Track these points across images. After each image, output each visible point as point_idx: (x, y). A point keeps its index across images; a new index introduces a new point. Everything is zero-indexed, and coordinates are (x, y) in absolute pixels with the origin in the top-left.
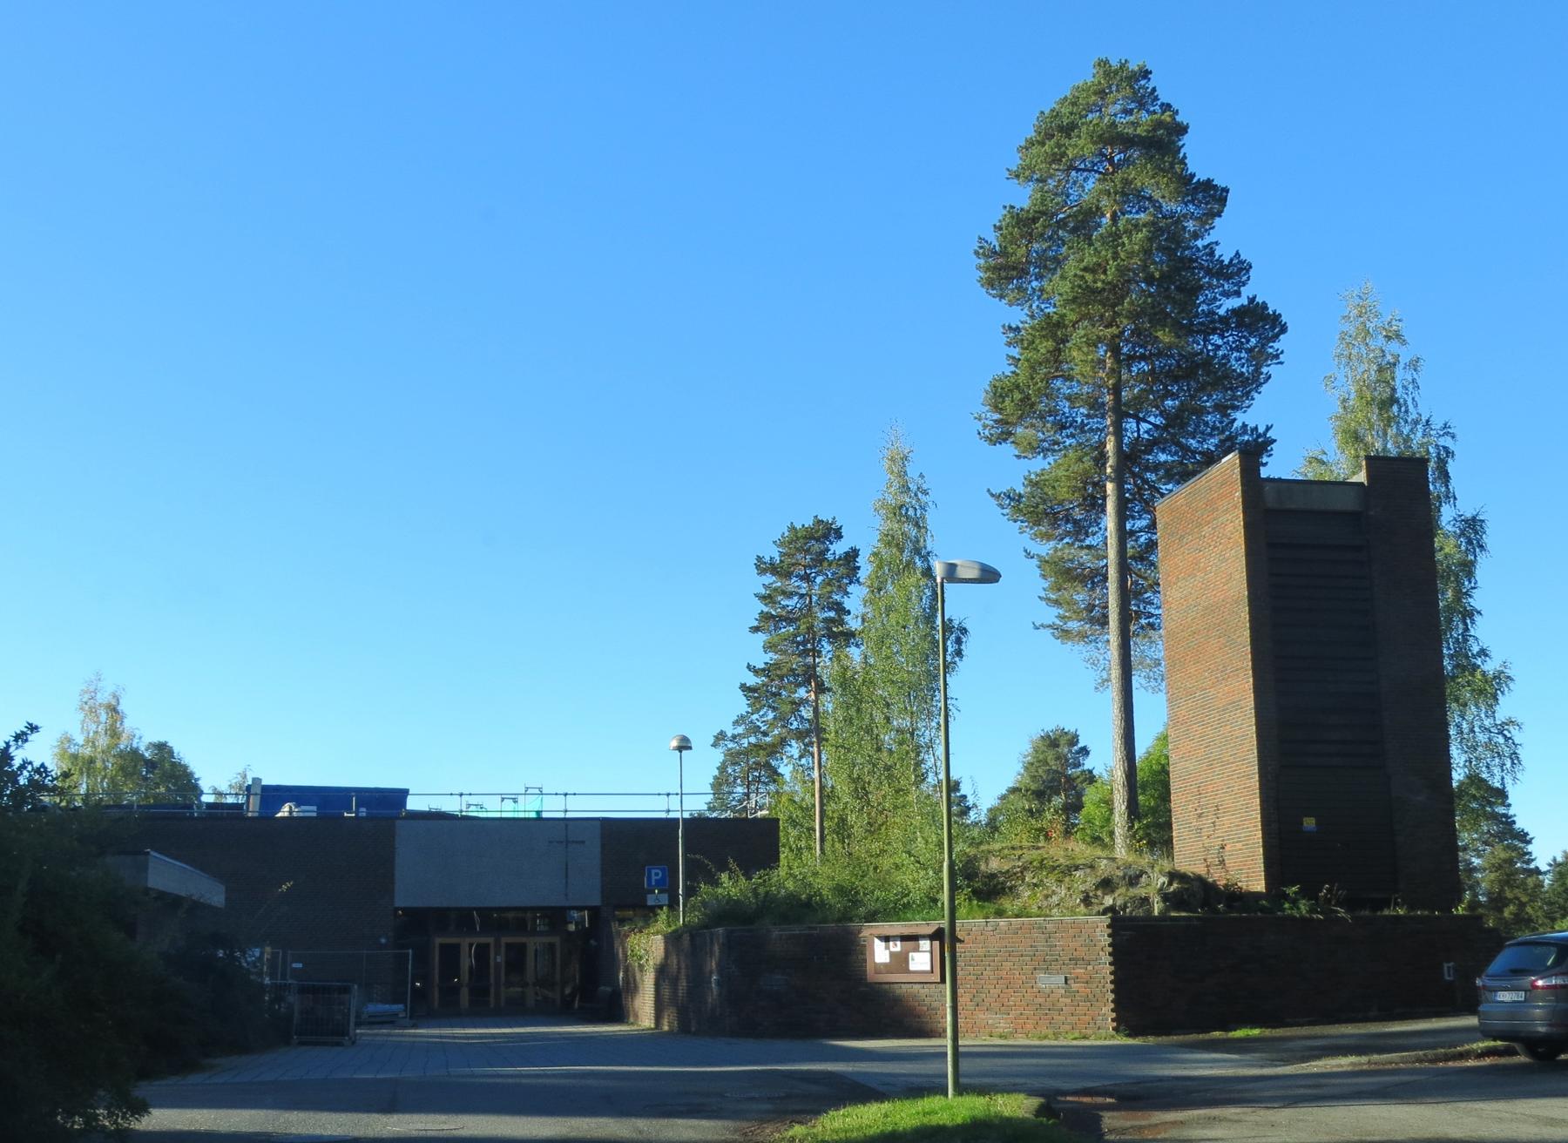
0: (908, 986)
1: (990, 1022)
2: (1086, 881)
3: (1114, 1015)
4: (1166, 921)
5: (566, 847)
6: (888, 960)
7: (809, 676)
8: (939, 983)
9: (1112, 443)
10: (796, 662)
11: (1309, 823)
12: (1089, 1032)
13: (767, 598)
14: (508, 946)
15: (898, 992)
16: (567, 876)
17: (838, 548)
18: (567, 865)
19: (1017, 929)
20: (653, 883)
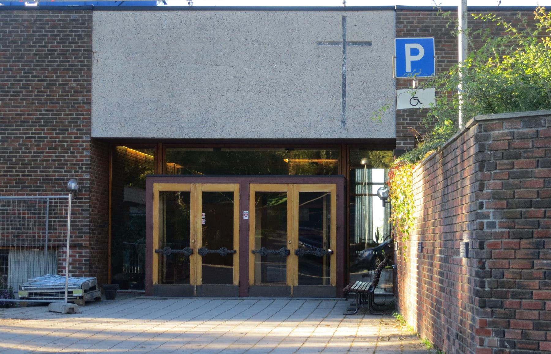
5: (344, 52)
14: (262, 197)
16: (344, 95)
18: (344, 78)
20: (408, 68)
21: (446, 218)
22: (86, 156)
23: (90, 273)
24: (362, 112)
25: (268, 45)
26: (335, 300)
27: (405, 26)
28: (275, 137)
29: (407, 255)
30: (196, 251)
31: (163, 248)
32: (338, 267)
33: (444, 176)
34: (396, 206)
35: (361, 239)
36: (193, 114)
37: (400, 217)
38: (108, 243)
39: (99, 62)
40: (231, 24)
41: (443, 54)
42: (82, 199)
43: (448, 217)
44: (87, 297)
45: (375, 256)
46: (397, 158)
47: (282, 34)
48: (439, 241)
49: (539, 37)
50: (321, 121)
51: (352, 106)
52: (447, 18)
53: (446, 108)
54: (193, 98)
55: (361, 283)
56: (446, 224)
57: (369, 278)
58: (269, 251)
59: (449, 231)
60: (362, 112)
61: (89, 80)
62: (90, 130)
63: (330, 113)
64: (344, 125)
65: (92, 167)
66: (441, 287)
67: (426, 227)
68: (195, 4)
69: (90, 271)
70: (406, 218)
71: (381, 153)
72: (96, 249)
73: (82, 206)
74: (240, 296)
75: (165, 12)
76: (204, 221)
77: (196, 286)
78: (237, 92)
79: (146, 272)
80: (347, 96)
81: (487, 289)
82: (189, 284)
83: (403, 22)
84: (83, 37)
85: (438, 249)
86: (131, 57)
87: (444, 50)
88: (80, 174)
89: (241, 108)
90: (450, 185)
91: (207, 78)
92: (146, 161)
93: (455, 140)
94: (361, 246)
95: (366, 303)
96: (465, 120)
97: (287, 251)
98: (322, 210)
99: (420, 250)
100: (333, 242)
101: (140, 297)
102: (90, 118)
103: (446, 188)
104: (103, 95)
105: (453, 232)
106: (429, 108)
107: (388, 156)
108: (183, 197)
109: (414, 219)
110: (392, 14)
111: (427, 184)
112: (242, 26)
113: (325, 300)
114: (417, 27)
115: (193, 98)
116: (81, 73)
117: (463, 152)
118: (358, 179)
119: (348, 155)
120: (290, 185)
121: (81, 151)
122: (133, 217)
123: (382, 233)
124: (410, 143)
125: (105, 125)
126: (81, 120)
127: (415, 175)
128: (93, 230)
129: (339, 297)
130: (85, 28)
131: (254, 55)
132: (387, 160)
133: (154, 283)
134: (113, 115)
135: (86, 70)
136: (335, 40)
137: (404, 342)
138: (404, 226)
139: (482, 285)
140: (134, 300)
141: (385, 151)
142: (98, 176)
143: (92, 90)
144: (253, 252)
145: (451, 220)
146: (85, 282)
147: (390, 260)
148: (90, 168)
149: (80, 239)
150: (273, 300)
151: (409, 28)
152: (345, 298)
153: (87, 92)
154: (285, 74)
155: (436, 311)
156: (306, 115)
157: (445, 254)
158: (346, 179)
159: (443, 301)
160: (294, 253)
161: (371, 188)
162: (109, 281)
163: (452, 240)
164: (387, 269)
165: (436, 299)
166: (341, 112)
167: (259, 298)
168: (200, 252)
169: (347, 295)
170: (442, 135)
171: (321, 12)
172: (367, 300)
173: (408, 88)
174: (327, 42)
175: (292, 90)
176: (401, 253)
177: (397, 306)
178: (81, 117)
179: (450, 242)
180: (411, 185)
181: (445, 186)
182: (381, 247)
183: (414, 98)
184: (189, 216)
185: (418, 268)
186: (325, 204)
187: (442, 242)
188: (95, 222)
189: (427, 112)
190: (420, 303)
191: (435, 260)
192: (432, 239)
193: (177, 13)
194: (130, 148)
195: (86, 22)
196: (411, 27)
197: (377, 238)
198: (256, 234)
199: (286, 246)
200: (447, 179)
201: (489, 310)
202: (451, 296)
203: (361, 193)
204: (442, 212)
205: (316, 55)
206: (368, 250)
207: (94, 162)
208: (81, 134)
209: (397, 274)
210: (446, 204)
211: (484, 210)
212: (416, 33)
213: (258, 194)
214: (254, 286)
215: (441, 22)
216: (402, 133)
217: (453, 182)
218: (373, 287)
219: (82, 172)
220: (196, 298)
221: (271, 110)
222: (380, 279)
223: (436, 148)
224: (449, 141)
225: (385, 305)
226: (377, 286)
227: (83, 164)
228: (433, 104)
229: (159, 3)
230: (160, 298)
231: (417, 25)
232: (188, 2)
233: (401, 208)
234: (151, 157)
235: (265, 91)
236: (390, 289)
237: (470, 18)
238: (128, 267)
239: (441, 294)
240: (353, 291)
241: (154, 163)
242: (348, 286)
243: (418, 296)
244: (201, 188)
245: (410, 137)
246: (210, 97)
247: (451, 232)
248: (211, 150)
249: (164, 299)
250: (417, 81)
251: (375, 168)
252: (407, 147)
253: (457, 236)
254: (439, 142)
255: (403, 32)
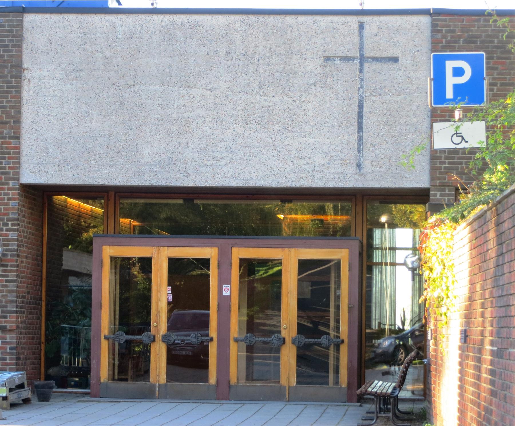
5: (361, 71)
16: (360, 128)
18: (361, 106)
20: (449, 94)
21: (500, 297)
22: (12, 209)
23: (16, 365)
24: (384, 152)
25: (258, 60)
26: (345, 405)
27: (444, 37)
28: (267, 185)
29: (444, 346)
30: (159, 337)
31: (114, 334)
32: (350, 361)
33: (498, 241)
34: (431, 279)
35: (380, 324)
36: (157, 154)
37: (435, 294)
38: (41, 325)
39: (31, 83)
40: (209, 32)
41: (495, 74)
42: (6, 266)
43: (502, 296)
44: (13, 398)
45: (397, 348)
46: (432, 215)
47: (276, 46)
48: (491, 328)
50: (329, 164)
51: (371, 144)
52: (504, 26)
53: (500, 148)
54: (157, 132)
55: (381, 383)
56: (499, 305)
57: (390, 377)
58: (257, 339)
59: (504, 315)
60: (384, 152)
61: (17, 106)
62: (18, 174)
63: (342, 152)
64: (360, 170)
65: (21, 224)
66: (491, 390)
67: (472, 309)
68: (161, 5)
69: (16, 363)
70: (445, 297)
71: (408, 207)
72: (25, 334)
73: (7, 276)
74: (218, 399)
75: (120, 16)
76: (170, 298)
77: (159, 385)
78: (215, 124)
79: (92, 366)
80: (364, 130)
82: (149, 382)
83: (440, 31)
84: (10, 48)
85: (488, 339)
86: (74, 75)
87: (496, 69)
88: (4, 232)
89: (221, 146)
90: (506, 252)
91: (175, 105)
92: (93, 216)
94: (380, 333)
95: (388, 410)
97: (282, 339)
98: (328, 283)
99: (463, 340)
100: (344, 328)
101: (83, 399)
102: (19, 158)
103: (501, 257)
104: (36, 127)
105: (509, 316)
106: (478, 148)
107: (417, 211)
108: (140, 264)
109: (455, 297)
110: (425, 21)
111: (473, 252)
112: (224, 35)
113: (332, 405)
114: (460, 37)
115: (157, 132)
116: (7, 97)
118: (377, 242)
119: (365, 209)
120: (287, 250)
121: (6, 201)
122: (74, 291)
123: (408, 318)
124: (449, 195)
125: (38, 166)
126: (7, 159)
127: (456, 238)
128: (22, 307)
129: (351, 402)
130: (13, 36)
131: (239, 74)
132: (415, 217)
133: (102, 381)
134: (49, 154)
135: (14, 93)
136: (349, 54)
138: (441, 306)
140: (76, 402)
141: (414, 205)
142: (28, 235)
143: (21, 120)
144: (236, 340)
145: (507, 301)
146: (10, 378)
147: (421, 353)
148: (19, 225)
149: (4, 320)
150: (262, 406)
151: (449, 38)
152: (359, 404)
153: (14, 122)
154: (281, 100)
155: (484, 423)
156: (308, 156)
157: (498, 345)
158: (361, 243)
159: (495, 409)
160: (291, 342)
161: (394, 254)
162: (42, 376)
163: (508, 327)
164: (416, 364)
165: (485, 407)
166: (356, 152)
167: (242, 402)
168: (164, 339)
169: (361, 399)
170: (496, 185)
171: (329, 16)
172: (389, 406)
173: (449, 121)
174: (338, 57)
175: (290, 122)
176: (436, 344)
177: (429, 414)
178: (7, 156)
179: (505, 329)
180: (451, 251)
181: (499, 254)
182: (407, 334)
183: (457, 133)
184: (150, 290)
185: (460, 364)
186: (333, 275)
187: (495, 330)
188: (24, 297)
189: (475, 153)
191: (485, 353)
192: (481, 325)
193: (137, 18)
194: (71, 198)
195: (14, 29)
196: (452, 37)
197: (403, 323)
198: (239, 315)
199: (279, 332)
200: (501, 244)
202: (507, 403)
203: (380, 261)
204: (495, 289)
205: (322, 75)
206: (389, 338)
207: (24, 217)
208: (6, 179)
209: (430, 371)
210: (501, 278)
212: (459, 46)
213: (242, 261)
214: (237, 386)
215: (493, 30)
216: (438, 181)
217: (510, 249)
218: (398, 389)
219: (7, 230)
220: (158, 401)
221: (261, 149)
222: (407, 378)
223: (488, 203)
224: (506, 193)
225: (413, 414)
226: (402, 388)
227: (8, 220)
228: (483, 142)
229: (112, 3)
230: (124, 400)
231: (461, 35)
232: (152, 2)
233: (437, 283)
234: (99, 211)
235: (254, 122)
236: (419, 391)
238: (66, 357)
239: (491, 400)
240: (370, 394)
241: (103, 220)
242: (363, 386)
243: (460, 402)
244: (166, 252)
245: (449, 186)
246: (180, 130)
247: (506, 317)
248: (181, 201)
249: (115, 402)
250: (461, 112)
251: (400, 228)
252: (445, 200)
254: (492, 194)
255: (440, 45)
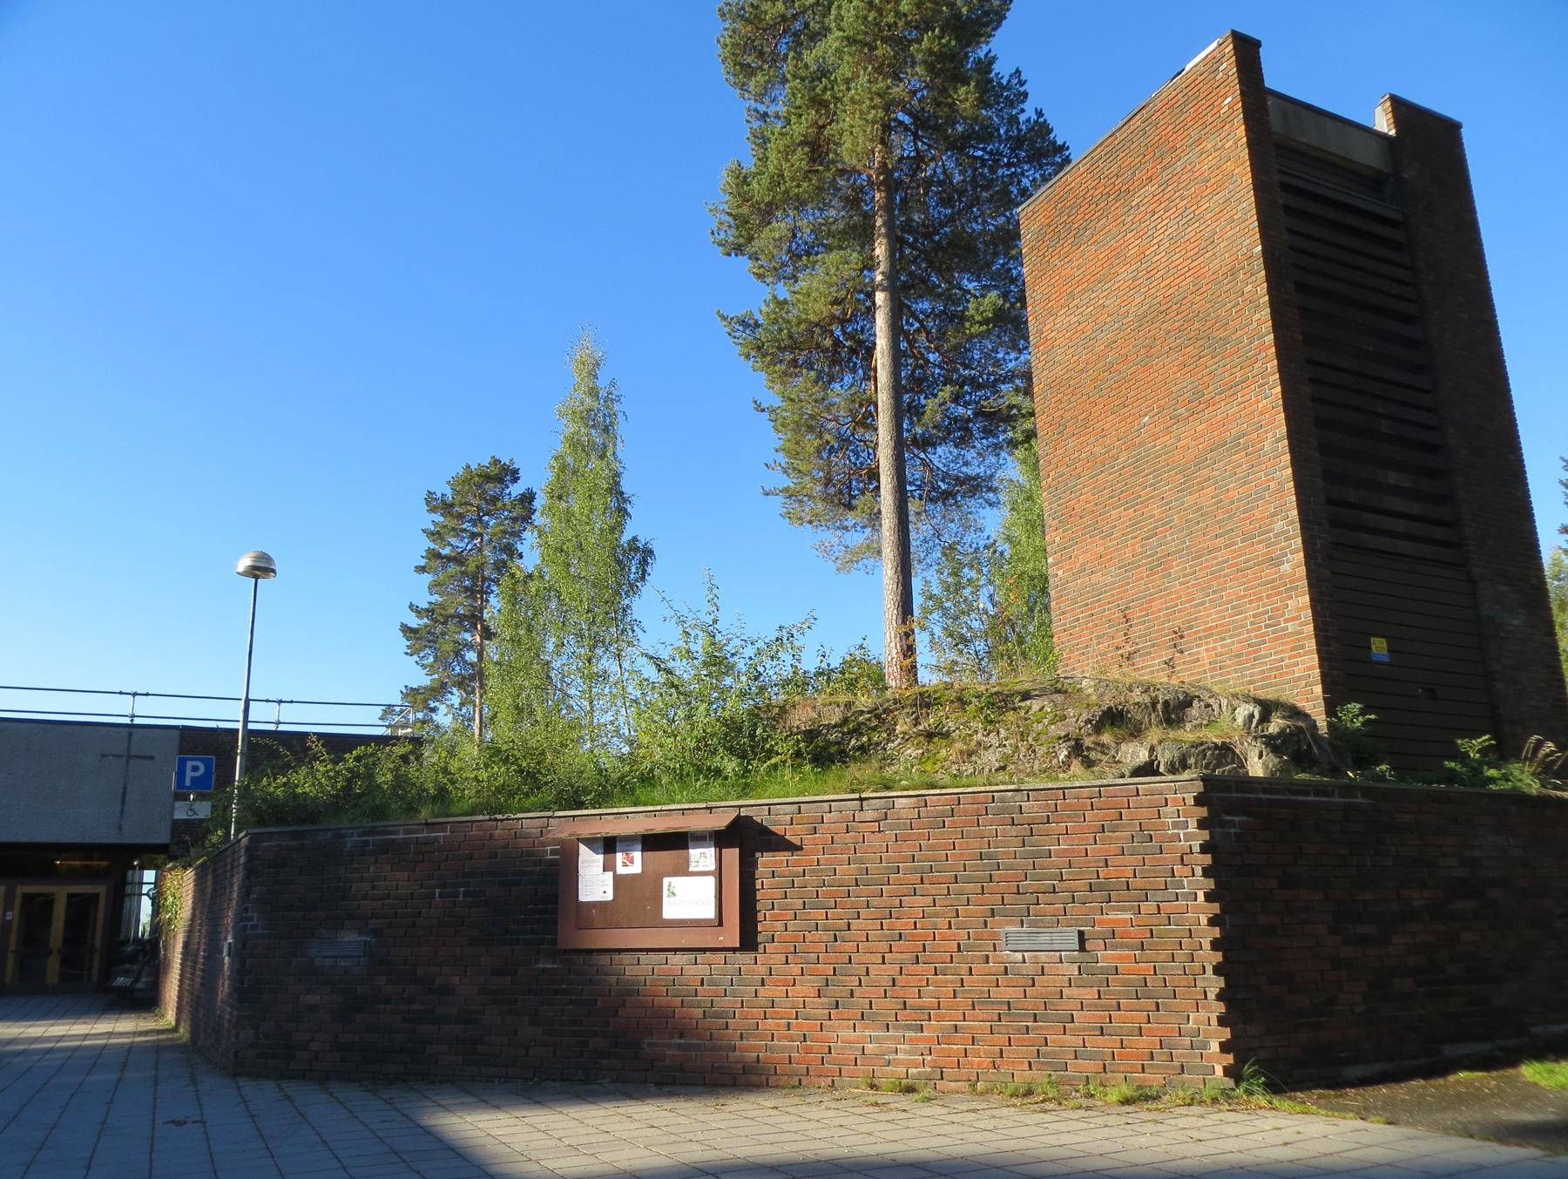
0: (654, 957)
1: (870, 1047)
2: (1064, 718)
3: (1226, 1033)
4: (1307, 794)
5: (127, 764)
6: (583, 898)
7: (474, 619)
8: (734, 950)
9: (883, 247)
10: (462, 606)
11: (1379, 646)
12: (1154, 1079)
13: (435, 535)
14: (28, 898)
15: (631, 971)
16: (123, 803)
17: (516, 490)
18: (125, 788)
19: (943, 815)
20: (188, 783)
49: (311, 760)
81: (246, 986)
93: (226, 849)
96: (237, 831)
117: (233, 861)
118: (129, 878)
132: (159, 861)
137: (161, 1037)
139: (242, 982)
144: (13, 952)
190: (180, 997)
201: (246, 1005)
211: (250, 914)
237: (250, 742)
253: (222, 937)
